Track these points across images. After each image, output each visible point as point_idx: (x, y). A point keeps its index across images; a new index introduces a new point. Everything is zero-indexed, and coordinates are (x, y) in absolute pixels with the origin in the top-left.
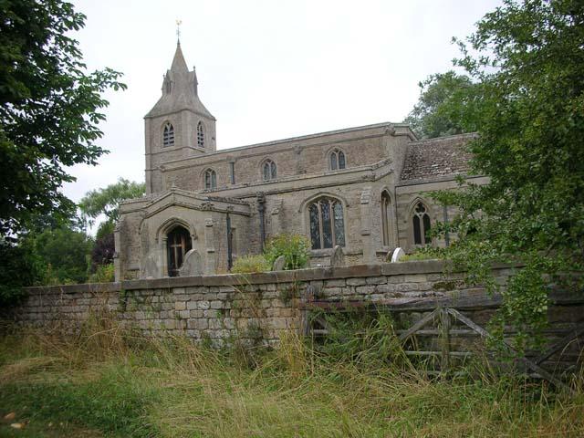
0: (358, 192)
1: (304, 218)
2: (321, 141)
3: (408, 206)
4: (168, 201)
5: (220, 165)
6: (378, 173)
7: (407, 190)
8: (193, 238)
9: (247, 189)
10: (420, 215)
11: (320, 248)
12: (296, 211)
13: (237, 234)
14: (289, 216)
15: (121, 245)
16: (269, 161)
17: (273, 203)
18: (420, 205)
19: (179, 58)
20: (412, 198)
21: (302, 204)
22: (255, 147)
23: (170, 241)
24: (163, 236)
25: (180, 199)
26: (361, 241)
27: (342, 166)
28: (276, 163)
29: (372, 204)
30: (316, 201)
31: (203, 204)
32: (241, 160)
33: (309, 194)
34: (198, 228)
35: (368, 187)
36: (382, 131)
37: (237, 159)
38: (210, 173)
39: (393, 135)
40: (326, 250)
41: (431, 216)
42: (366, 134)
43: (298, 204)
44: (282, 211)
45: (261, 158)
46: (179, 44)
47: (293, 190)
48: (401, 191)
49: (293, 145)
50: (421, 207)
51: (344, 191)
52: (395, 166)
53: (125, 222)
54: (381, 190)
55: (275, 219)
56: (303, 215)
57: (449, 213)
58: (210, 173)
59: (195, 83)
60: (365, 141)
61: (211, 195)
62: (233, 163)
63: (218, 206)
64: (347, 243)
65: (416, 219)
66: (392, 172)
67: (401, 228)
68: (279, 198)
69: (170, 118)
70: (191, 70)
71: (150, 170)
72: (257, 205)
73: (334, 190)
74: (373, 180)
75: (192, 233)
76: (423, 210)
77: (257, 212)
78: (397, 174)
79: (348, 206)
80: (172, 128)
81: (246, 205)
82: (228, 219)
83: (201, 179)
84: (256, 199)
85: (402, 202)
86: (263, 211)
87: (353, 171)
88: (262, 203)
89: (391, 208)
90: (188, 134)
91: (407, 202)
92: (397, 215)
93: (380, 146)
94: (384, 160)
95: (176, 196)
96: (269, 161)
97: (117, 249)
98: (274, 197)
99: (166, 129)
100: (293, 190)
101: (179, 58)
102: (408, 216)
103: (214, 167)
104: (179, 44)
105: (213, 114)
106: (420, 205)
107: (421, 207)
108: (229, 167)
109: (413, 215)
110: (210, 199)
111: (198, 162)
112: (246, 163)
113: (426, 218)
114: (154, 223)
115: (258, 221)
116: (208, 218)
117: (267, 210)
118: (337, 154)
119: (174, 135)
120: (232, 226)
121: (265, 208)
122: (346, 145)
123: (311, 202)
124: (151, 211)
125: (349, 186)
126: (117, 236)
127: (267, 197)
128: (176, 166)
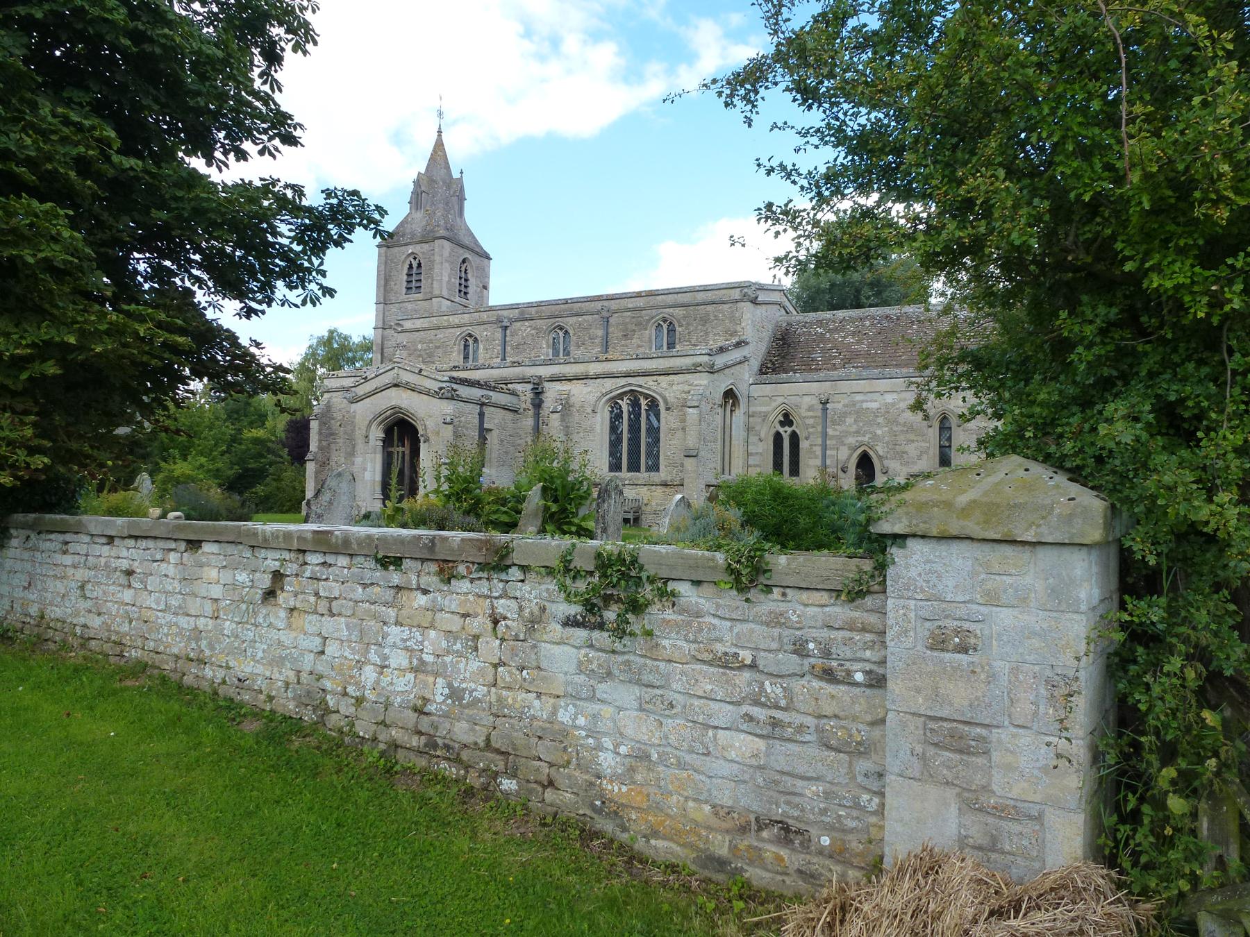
0: (686, 388)
1: (601, 422)
2: (640, 302)
3: (765, 417)
4: (387, 379)
5: (486, 330)
6: (720, 360)
7: (768, 389)
8: (422, 439)
9: (518, 370)
10: (786, 432)
11: (620, 470)
12: (589, 410)
13: (493, 439)
14: (576, 417)
15: (320, 441)
16: (561, 329)
17: (553, 392)
18: (786, 415)
19: (439, 146)
20: (774, 405)
21: (599, 399)
22: (539, 304)
23: (387, 441)
24: (377, 433)
25: (406, 377)
26: (682, 465)
27: (671, 345)
28: (571, 332)
29: (705, 407)
30: (621, 396)
31: (441, 389)
32: (519, 324)
33: (609, 384)
34: (430, 424)
35: (702, 380)
36: (736, 294)
37: (512, 321)
38: (471, 341)
39: (754, 302)
40: (630, 474)
41: (801, 434)
42: (709, 296)
43: (592, 399)
44: (566, 406)
45: (458, 331)
46: (440, 132)
47: (586, 377)
48: (757, 391)
49: (599, 305)
50: (787, 420)
51: (663, 385)
52: (757, 350)
53: (328, 406)
54: (723, 389)
55: (555, 420)
56: (598, 417)
57: (830, 432)
58: (471, 341)
59: (461, 198)
60: (709, 308)
61: (455, 374)
62: (506, 328)
63: (464, 391)
64: (662, 467)
65: (778, 438)
66: (745, 360)
67: (752, 449)
68: (565, 387)
69: (417, 249)
70: (456, 175)
71: (383, 325)
72: (530, 396)
73: (649, 382)
74: (712, 370)
75: (421, 432)
76: (790, 423)
77: (531, 407)
78: (755, 364)
79: (668, 409)
80: (419, 265)
81: (514, 393)
82: (481, 415)
83: (456, 348)
84: (530, 386)
85: (759, 409)
86: (538, 404)
87: (692, 352)
88: (538, 393)
89: (739, 416)
90: (442, 276)
91: (764, 409)
92: (749, 429)
93: (732, 318)
94: (737, 339)
95: (401, 372)
96: (470, 336)
97: (313, 447)
98: (557, 386)
99: (411, 266)
100: (586, 377)
101: (439, 146)
102: (767, 433)
103: (476, 332)
104: (440, 132)
105: (487, 247)
106: (786, 415)
107: (787, 420)
108: (499, 334)
109: (773, 431)
110: (453, 380)
111: (455, 320)
112: (525, 329)
113: (794, 438)
114: (364, 411)
115: (529, 422)
116: (448, 408)
117: (544, 405)
118: (665, 326)
119: (423, 282)
120: (486, 426)
121: (541, 401)
122: (679, 312)
123: (612, 398)
124: (361, 391)
125: (672, 377)
126: (314, 425)
127: (546, 385)
128: (418, 324)
